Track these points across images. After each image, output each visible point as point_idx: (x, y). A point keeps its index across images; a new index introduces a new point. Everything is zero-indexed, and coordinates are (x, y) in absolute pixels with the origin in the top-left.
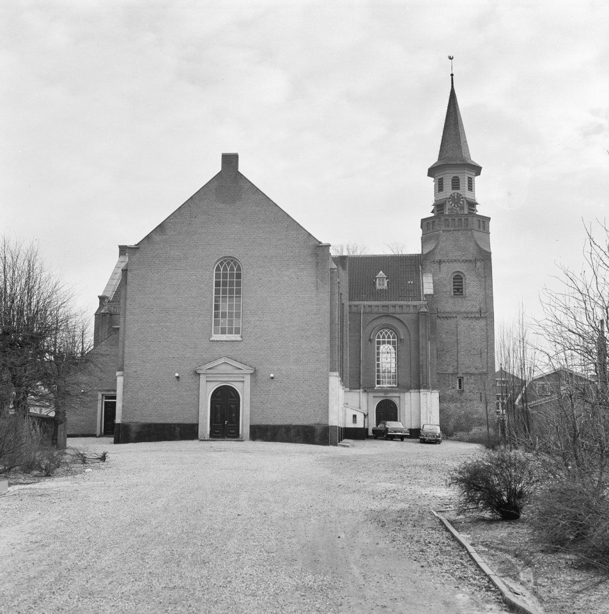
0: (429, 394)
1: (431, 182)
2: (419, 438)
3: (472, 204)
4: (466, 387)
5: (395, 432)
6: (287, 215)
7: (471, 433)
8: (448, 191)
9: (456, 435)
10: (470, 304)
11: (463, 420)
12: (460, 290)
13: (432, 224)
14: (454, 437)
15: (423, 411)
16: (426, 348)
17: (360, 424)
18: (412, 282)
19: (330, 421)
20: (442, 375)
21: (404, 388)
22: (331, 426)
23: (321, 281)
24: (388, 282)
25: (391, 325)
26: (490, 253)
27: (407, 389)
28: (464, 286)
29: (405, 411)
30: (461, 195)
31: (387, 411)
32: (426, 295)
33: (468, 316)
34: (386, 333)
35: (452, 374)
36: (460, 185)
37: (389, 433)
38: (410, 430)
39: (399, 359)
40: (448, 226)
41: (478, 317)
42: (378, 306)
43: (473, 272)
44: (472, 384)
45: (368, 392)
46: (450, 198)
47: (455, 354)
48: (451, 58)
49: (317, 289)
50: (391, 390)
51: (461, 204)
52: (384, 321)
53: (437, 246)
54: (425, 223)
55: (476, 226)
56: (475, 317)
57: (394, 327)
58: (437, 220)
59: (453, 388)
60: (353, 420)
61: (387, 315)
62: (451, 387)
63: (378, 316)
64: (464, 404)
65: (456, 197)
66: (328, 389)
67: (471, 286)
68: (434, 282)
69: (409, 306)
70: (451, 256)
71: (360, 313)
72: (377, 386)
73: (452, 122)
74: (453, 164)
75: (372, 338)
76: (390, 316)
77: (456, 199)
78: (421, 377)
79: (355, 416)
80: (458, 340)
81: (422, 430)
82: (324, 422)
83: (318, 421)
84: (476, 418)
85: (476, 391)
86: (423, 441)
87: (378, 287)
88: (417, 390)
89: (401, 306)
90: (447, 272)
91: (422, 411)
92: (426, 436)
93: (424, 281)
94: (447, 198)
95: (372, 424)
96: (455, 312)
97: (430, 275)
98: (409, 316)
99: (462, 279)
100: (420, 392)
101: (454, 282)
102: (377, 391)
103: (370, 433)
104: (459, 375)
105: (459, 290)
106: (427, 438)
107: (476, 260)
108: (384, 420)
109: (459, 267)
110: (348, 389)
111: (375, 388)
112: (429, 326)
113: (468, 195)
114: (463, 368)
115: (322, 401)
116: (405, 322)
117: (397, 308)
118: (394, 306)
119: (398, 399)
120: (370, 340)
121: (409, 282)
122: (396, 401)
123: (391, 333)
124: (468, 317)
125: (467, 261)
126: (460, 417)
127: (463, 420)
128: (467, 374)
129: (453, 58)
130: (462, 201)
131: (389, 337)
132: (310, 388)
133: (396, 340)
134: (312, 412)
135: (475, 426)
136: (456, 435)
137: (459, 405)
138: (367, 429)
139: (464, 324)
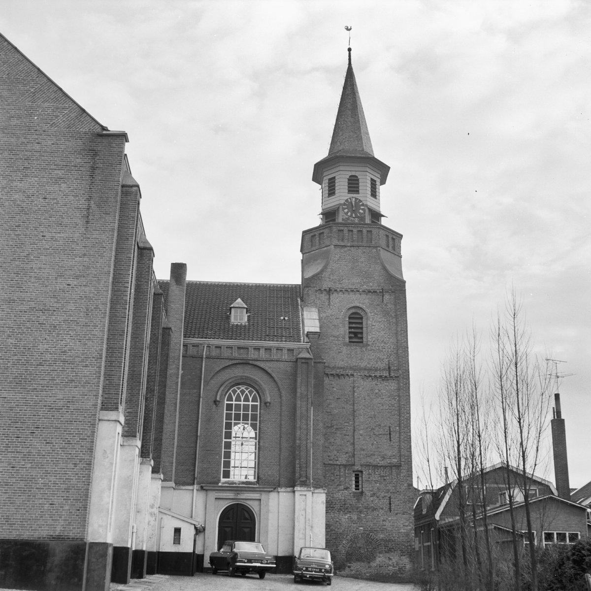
0: (309, 494)
1: (317, 190)
2: (293, 574)
3: (376, 216)
4: (366, 487)
5: (250, 561)
6: (39, 69)
7: (373, 564)
8: (342, 194)
9: (349, 567)
10: (372, 356)
11: (361, 543)
12: (359, 336)
13: (319, 237)
14: (347, 571)
15: (299, 525)
16: (307, 418)
17: (186, 546)
18: (286, 318)
19: (90, 529)
20: (330, 466)
21: (265, 482)
22: (93, 545)
23: (99, 206)
24: (249, 317)
25: (251, 379)
26: (404, 282)
27: (274, 486)
28: (364, 329)
29: (267, 526)
30: (360, 201)
31: (238, 522)
32: (308, 334)
33: (370, 374)
34: (243, 392)
35: (345, 466)
36: (360, 184)
37: (238, 564)
38: (277, 558)
39: (262, 435)
40: (343, 240)
41: (386, 377)
42: (230, 347)
43: (379, 308)
44: (376, 482)
45: (207, 490)
46: (344, 204)
47: (351, 434)
48: (348, 29)
49: (87, 222)
50: (246, 487)
51: (360, 213)
52: (239, 372)
53: (325, 267)
54: (308, 237)
55: (383, 243)
56: (381, 377)
57: (256, 382)
58: (326, 231)
59: (346, 488)
60: (175, 540)
61: (245, 363)
62: (342, 487)
63: (231, 363)
64: (362, 515)
65: (353, 203)
66: (91, 450)
67: (375, 327)
68: (320, 320)
69: (282, 350)
70: (346, 284)
71: (202, 358)
72: (223, 480)
73: (349, 106)
74: (349, 161)
75: (218, 399)
76: (249, 364)
77: (354, 206)
78: (297, 466)
79: (178, 531)
80: (354, 411)
81: (299, 558)
82: (73, 532)
83: (58, 530)
84: (382, 540)
85: (383, 494)
86: (301, 580)
87: (233, 320)
88: (289, 489)
89: (268, 349)
90: (341, 305)
91: (296, 524)
92: (307, 570)
93: (305, 316)
94: (340, 204)
95: (211, 546)
96: (351, 368)
97: (314, 309)
98: (281, 365)
99: (362, 318)
100: (294, 492)
101: (350, 323)
102: (223, 489)
103: (207, 563)
104: (356, 468)
105: (356, 335)
106: (308, 574)
107: (383, 292)
108: (232, 539)
109: (357, 300)
110: (172, 484)
111: (220, 484)
112: (312, 381)
113: (370, 202)
114: (362, 457)
115: (74, 481)
116: (273, 375)
117: (262, 351)
118: (257, 349)
119: (257, 503)
120: (215, 402)
121: (282, 318)
122: (254, 506)
123: (251, 392)
124: (370, 376)
125: (369, 292)
126: (356, 537)
127: (361, 543)
128: (368, 465)
129: (350, 29)
130: (362, 209)
131: (246, 399)
132: (48, 448)
133: (258, 404)
134: (46, 507)
135: (380, 553)
136: (349, 567)
137: (355, 517)
138: (202, 556)
139: (364, 386)
